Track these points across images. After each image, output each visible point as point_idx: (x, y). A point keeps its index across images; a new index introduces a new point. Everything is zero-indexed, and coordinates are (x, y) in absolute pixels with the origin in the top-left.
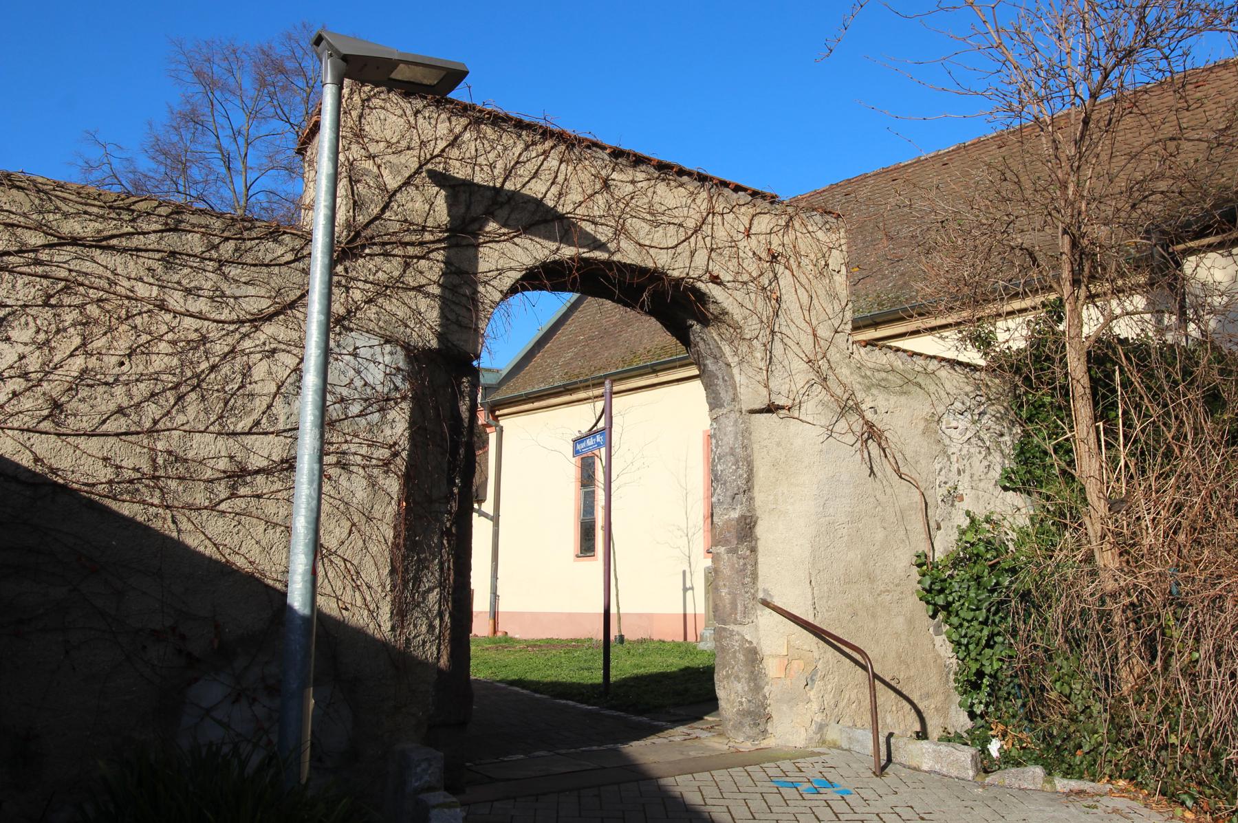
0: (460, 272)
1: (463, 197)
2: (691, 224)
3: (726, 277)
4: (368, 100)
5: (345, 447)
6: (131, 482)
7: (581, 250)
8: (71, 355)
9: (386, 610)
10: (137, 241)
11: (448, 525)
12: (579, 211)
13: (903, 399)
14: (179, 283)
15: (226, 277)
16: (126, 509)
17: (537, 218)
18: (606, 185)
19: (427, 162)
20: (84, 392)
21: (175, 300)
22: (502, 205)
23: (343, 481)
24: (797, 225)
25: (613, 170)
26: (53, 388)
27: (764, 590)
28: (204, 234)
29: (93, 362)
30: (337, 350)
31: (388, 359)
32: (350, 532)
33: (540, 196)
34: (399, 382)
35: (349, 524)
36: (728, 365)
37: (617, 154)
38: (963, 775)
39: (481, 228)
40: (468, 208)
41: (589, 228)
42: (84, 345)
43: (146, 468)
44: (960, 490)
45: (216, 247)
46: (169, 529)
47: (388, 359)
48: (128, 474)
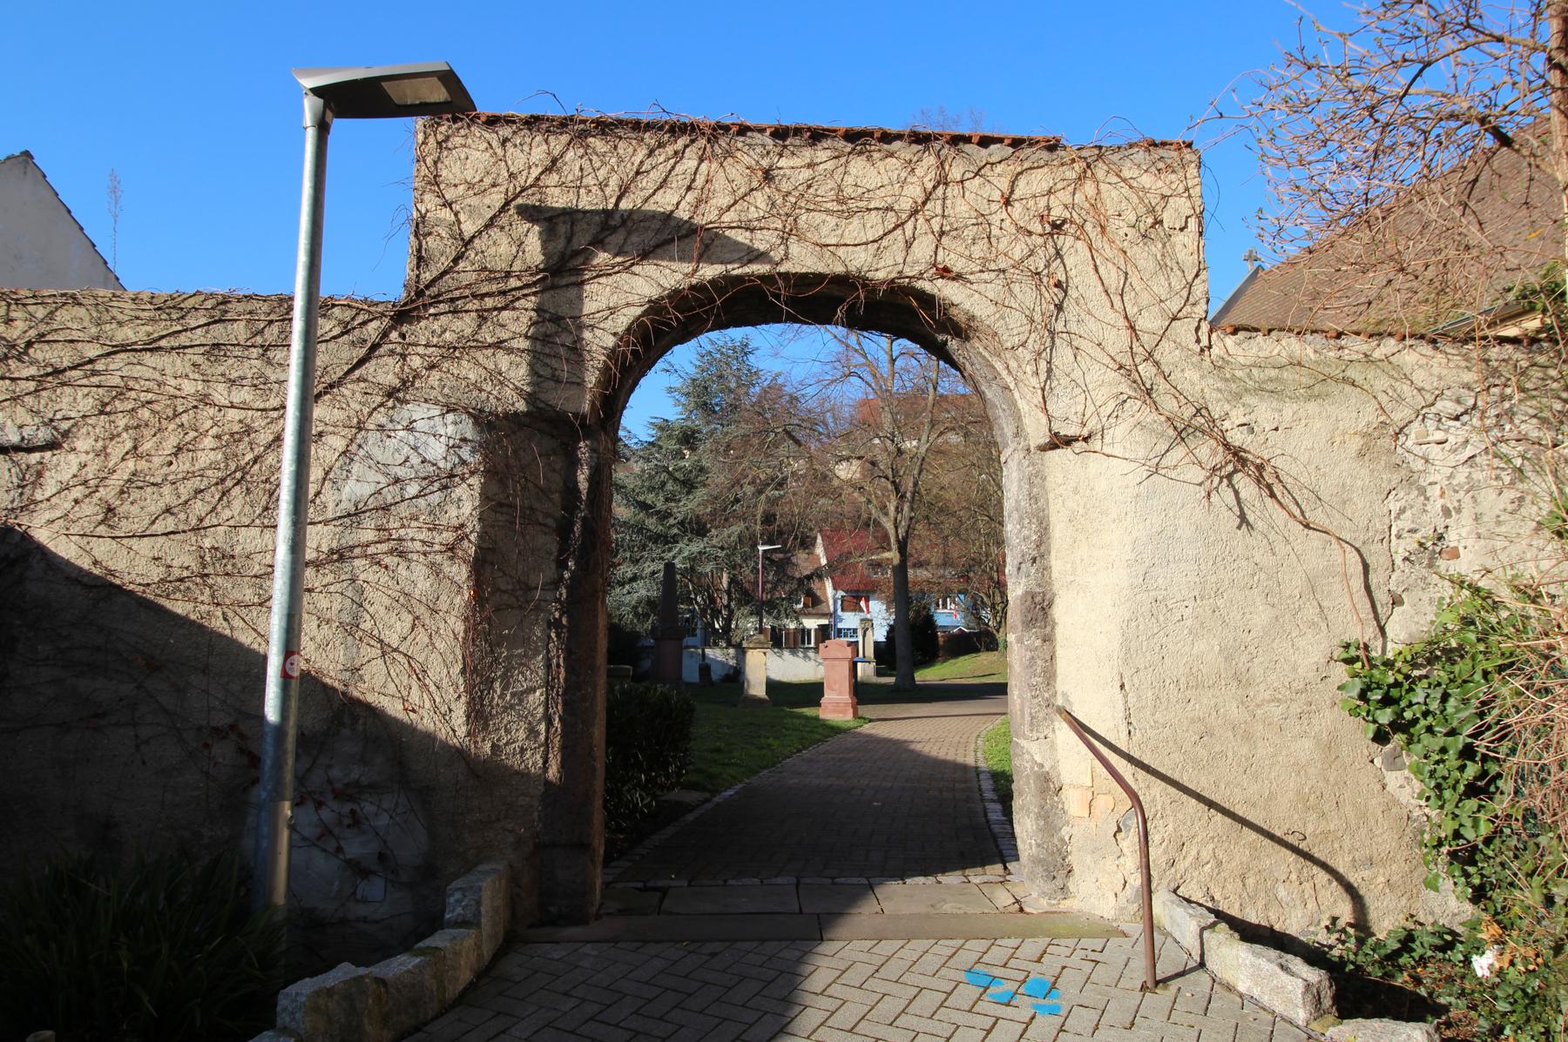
0: (557, 319)
1: (563, 229)
2: (905, 204)
3: (958, 266)
4: (447, 138)
5: (402, 532)
6: (181, 580)
7: (730, 267)
8: (123, 459)
9: (460, 710)
10: (183, 339)
11: (557, 615)
12: (726, 218)
13: (1312, 407)
14: (223, 375)
15: (269, 362)
16: (179, 607)
17: (663, 235)
18: (768, 176)
19: (516, 197)
20: (135, 494)
21: (220, 394)
22: (614, 229)
23: (402, 570)
24: (1100, 174)
25: (781, 155)
26: (108, 493)
27: (1064, 694)
28: (249, 321)
29: (142, 465)
30: (390, 426)
31: (450, 429)
32: (413, 627)
33: (670, 208)
34: (465, 453)
35: (411, 617)
36: (1007, 388)
37: (780, 134)
38: (1291, 1014)
39: (587, 261)
40: (569, 240)
41: (741, 237)
42: (135, 448)
43: (195, 567)
44: (1452, 539)
45: (261, 332)
46: (217, 624)
47: (450, 429)
48: (177, 573)
